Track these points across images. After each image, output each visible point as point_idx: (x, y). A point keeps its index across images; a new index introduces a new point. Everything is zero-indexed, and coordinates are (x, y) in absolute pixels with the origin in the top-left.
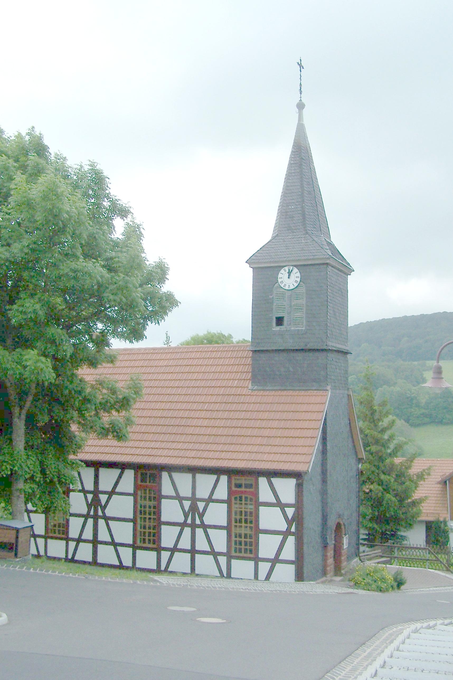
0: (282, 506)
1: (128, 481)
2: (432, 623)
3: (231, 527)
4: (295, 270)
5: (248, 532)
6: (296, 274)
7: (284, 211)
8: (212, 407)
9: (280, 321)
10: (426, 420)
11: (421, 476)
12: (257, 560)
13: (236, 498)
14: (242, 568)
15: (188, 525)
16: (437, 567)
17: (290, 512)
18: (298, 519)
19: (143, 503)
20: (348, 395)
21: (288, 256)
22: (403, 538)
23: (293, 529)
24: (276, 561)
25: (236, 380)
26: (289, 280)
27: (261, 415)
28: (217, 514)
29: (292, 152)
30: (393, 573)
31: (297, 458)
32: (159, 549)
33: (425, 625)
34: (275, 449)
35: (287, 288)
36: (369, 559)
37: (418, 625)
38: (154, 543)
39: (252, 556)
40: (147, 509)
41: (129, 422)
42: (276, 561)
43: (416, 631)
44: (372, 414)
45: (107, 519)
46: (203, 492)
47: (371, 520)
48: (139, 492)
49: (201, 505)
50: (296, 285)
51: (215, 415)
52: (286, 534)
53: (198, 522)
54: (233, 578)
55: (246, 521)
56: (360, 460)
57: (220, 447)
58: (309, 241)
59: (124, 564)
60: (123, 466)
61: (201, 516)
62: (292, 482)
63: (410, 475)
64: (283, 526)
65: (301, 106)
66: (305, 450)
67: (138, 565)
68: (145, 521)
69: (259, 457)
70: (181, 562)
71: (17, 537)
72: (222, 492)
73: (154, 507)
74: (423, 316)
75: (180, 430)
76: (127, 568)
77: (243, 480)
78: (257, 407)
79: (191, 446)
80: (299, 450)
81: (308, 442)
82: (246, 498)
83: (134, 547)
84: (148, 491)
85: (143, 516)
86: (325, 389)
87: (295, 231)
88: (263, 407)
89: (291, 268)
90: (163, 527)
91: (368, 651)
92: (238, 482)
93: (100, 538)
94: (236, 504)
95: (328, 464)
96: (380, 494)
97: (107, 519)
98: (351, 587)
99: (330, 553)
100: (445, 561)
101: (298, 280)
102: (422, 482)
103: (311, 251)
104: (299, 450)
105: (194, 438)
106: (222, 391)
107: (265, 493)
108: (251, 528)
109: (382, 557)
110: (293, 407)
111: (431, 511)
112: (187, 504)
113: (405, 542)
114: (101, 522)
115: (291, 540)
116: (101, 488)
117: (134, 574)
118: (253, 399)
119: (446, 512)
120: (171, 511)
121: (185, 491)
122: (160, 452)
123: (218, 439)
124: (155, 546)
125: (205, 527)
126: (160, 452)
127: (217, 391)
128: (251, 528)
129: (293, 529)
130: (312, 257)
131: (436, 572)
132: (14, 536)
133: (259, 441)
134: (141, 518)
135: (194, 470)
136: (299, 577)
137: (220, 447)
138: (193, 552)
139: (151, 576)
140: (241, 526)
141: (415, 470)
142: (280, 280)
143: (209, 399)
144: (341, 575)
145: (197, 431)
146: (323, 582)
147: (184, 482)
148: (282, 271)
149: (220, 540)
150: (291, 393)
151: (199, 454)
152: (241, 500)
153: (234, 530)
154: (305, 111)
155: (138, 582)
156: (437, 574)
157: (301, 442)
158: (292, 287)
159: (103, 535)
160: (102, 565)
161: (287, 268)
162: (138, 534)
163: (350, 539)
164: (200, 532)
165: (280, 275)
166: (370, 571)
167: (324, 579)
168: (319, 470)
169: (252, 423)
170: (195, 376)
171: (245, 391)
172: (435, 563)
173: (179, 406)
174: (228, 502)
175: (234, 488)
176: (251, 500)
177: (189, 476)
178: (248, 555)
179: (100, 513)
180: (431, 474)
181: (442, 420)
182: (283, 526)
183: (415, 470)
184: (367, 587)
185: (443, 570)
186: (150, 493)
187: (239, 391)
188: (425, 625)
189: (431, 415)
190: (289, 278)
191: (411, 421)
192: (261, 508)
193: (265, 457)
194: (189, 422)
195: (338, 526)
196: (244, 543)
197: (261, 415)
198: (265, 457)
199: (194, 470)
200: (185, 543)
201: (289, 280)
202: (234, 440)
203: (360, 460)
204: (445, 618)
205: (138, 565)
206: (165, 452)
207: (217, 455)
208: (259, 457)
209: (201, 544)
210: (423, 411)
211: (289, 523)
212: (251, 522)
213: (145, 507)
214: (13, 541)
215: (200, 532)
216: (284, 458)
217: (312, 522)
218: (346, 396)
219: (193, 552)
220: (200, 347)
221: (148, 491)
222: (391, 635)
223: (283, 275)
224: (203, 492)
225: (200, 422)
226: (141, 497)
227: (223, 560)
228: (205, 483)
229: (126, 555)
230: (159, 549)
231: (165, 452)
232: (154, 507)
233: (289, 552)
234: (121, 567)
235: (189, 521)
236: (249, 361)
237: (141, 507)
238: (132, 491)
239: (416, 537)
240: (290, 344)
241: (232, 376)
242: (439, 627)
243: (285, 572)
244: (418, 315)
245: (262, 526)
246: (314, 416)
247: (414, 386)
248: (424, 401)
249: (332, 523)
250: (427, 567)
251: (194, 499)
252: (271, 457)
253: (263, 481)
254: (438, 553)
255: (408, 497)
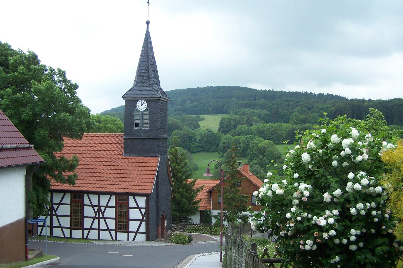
0: (140, 209)
1: (67, 199)
2: (205, 254)
3: (117, 219)
4: (145, 102)
5: (125, 220)
6: (145, 104)
7: (139, 73)
8: (106, 164)
9: (137, 125)
10: (200, 149)
11: (198, 190)
12: (129, 232)
13: (119, 206)
14: (122, 236)
15: (97, 218)
16: (206, 233)
17: (143, 211)
18: (147, 214)
19: (75, 208)
20: (167, 157)
21: (141, 95)
22: (191, 219)
23: (145, 219)
24: (137, 232)
25: (116, 151)
26: (142, 106)
27: (129, 168)
28: (110, 213)
29: (143, 44)
30: (188, 236)
31: (146, 188)
32: (83, 229)
33: (203, 254)
34: (136, 184)
35: (141, 110)
36: (176, 230)
37: (200, 255)
38: (80, 226)
39: (126, 231)
40: (77, 211)
41: (75, 176)
42: (137, 232)
43: (199, 256)
44: (176, 160)
45: (105, 219)
46: (104, 202)
47: (175, 211)
48: (73, 204)
49: (103, 209)
50: (145, 109)
51: (107, 167)
52: (141, 221)
53: (101, 216)
54: (101, 240)
55: (123, 216)
56: (172, 185)
57: (111, 183)
58: (151, 89)
59: (66, 236)
60: (110, 194)
61: (103, 213)
62: (144, 198)
63: (193, 189)
64: (141, 218)
65: (148, 23)
66: (150, 184)
67: (73, 237)
68: (76, 217)
69: (129, 187)
70: (93, 234)
71: (33, 228)
72: (112, 203)
73: (81, 210)
74: (198, 89)
75: (92, 174)
76: (68, 238)
77: (122, 197)
78: (127, 164)
79: (97, 182)
80: (147, 184)
81: (151, 180)
82: (124, 205)
83: (71, 228)
84: (77, 203)
85: (75, 214)
86: (158, 156)
87: (145, 83)
88: (130, 164)
89: (143, 101)
90: (85, 219)
91: (184, 262)
92: (120, 198)
93: (54, 225)
94: (118, 208)
95: (159, 189)
96: (180, 199)
97: (57, 216)
98: (170, 243)
99: (160, 228)
100: (209, 230)
101: (146, 106)
102: (199, 193)
103: (152, 94)
104: (147, 184)
105: (99, 178)
106: (110, 156)
107: (132, 203)
108: (126, 218)
109: (181, 229)
110: (143, 165)
111: (203, 206)
112: (96, 208)
113: (191, 221)
114: (55, 218)
115: (144, 223)
116: (54, 202)
117: (71, 240)
118: (125, 160)
119: (210, 206)
120: (88, 211)
121: (95, 203)
122: (83, 185)
123: (110, 179)
124: (81, 227)
125: (105, 219)
126: (83, 185)
127: (107, 156)
128: (126, 218)
129: (145, 219)
130: (152, 97)
131: (206, 235)
132: (32, 227)
133: (128, 180)
134: (74, 215)
135: (99, 193)
136: (148, 239)
137: (111, 183)
138: (99, 230)
139: (90, 241)
140: (121, 218)
141: (196, 187)
142: (137, 106)
143: (104, 160)
144: (164, 238)
145: (99, 175)
146: (158, 241)
147: (95, 199)
148: (139, 102)
149: (112, 224)
150: (142, 158)
151: (102, 186)
152: (121, 206)
153: (118, 220)
154: (150, 25)
155: (87, 243)
156: (206, 236)
157: (148, 180)
158: (143, 110)
159: (55, 223)
160: (74, 238)
161: (141, 101)
162: (73, 222)
163: (167, 222)
164: (102, 221)
165: (137, 104)
166: (178, 236)
167: (158, 240)
168: (155, 192)
169: (125, 172)
170: (97, 149)
171: (121, 157)
172: (205, 231)
173: (90, 163)
174: (115, 207)
175: (118, 201)
176: (126, 206)
177: (97, 196)
178: (125, 230)
179: (54, 213)
180: (204, 189)
181: (208, 150)
182: (141, 218)
183: (196, 187)
184: (177, 242)
185: (208, 234)
186: (78, 204)
187: (118, 156)
188: (202, 254)
189: (203, 146)
190: (142, 105)
191: (191, 150)
192: (130, 210)
193: (132, 187)
194: (96, 171)
195: (163, 216)
196: (122, 224)
197: (129, 168)
198: (132, 187)
199: (99, 193)
200: (95, 226)
201: (142, 106)
202: (118, 179)
203: (172, 185)
204: (209, 253)
205: (73, 237)
206: (85, 185)
207: (110, 186)
208: (129, 187)
209: (103, 226)
210: (198, 144)
211: (143, 216)
212: (126, 216)
213: (76, 210)
214: (31, 229)
215: (102, 221)
216: (140, 188)
217: (153, 215)
218: (166, 158)
219: (99, 230)
220: (98, 135)
221: (77, 203)
222: (191, 258)
223: (139, 104)
224: (104, 202)
225: (101, 171)
226: (74, 206)
227: (113, 233)
228: (104, 200)
229: (67, 232)
230: (83, 229)
231: (85, 185)
232: (81, 210)
233: (143, 228)
234: (65, 237)
235: (97, 216)
236: (122, 142)
237: (74, 210)
238: (69, 203)
239: (196, 219)
240: (142, 135)
241: (115, 149)
242: (207, 255)
243: (141, 238)
244: (258, 90)
245: (130, 218)
246: (153, 169)
247: (193, 130)
248: (198, 139)
249: (161, 214)
250: (201, 232)
251: (99, 206)
252: (135, 187)
253: (131, 198)
254: (206, 226)
255: (192, 200)
